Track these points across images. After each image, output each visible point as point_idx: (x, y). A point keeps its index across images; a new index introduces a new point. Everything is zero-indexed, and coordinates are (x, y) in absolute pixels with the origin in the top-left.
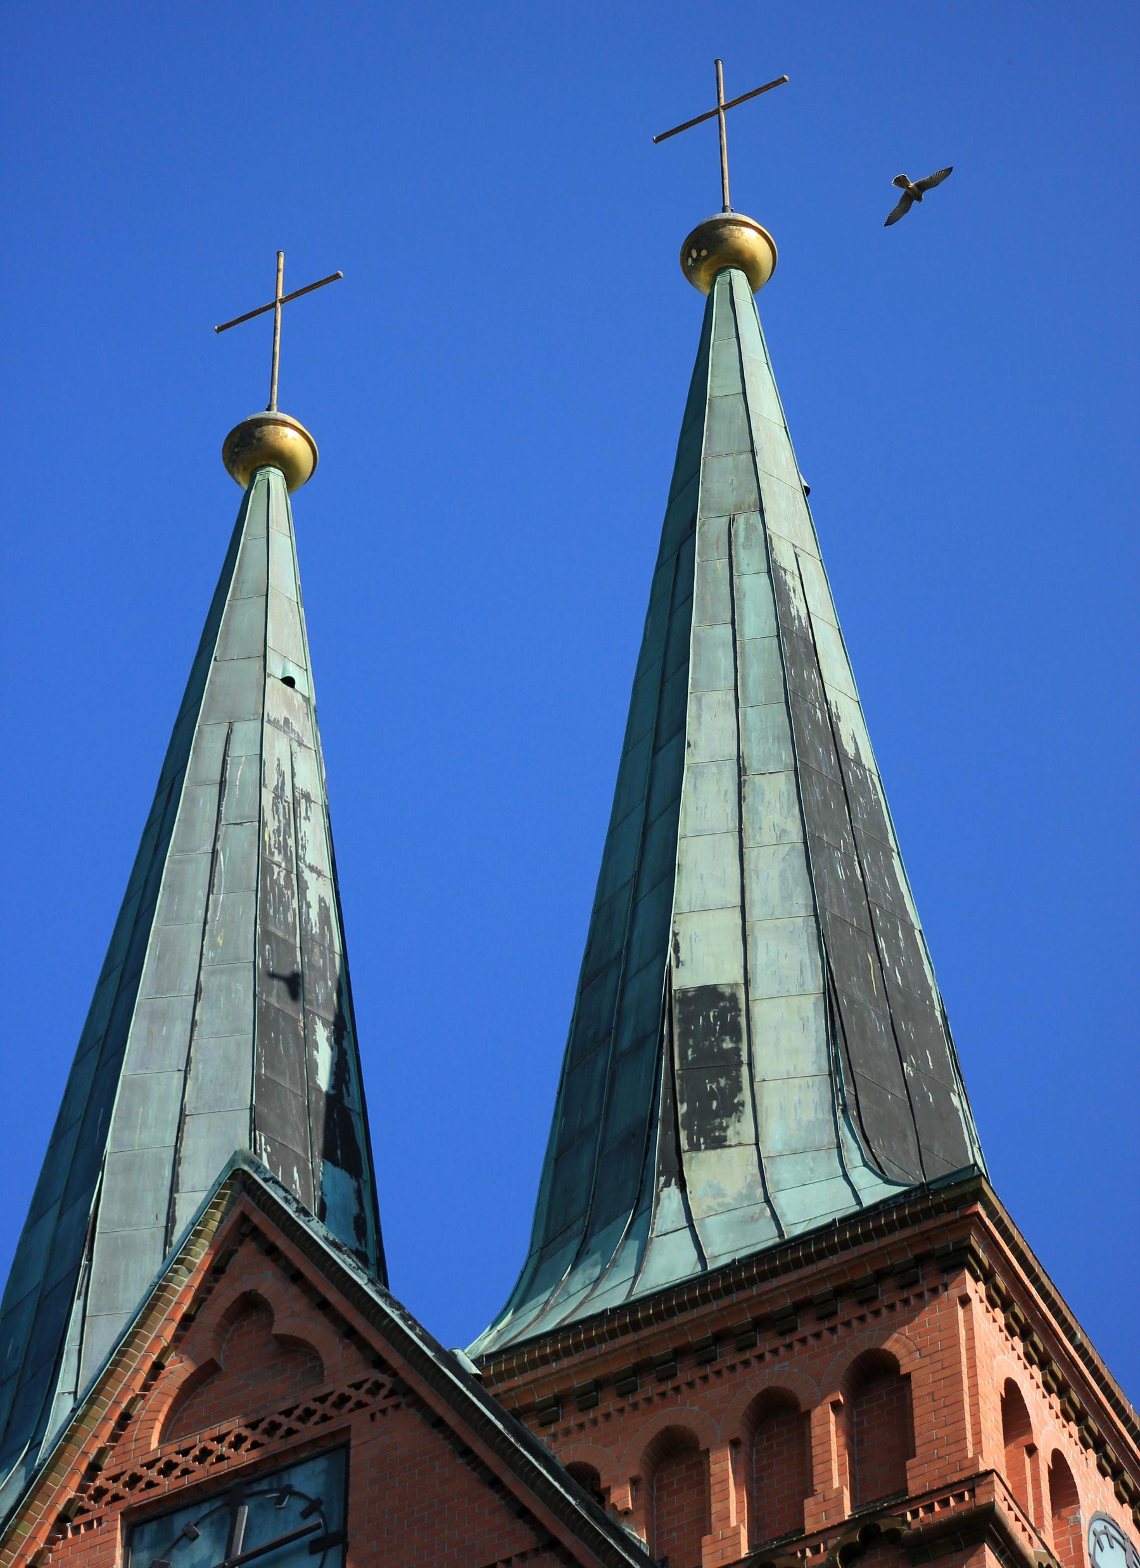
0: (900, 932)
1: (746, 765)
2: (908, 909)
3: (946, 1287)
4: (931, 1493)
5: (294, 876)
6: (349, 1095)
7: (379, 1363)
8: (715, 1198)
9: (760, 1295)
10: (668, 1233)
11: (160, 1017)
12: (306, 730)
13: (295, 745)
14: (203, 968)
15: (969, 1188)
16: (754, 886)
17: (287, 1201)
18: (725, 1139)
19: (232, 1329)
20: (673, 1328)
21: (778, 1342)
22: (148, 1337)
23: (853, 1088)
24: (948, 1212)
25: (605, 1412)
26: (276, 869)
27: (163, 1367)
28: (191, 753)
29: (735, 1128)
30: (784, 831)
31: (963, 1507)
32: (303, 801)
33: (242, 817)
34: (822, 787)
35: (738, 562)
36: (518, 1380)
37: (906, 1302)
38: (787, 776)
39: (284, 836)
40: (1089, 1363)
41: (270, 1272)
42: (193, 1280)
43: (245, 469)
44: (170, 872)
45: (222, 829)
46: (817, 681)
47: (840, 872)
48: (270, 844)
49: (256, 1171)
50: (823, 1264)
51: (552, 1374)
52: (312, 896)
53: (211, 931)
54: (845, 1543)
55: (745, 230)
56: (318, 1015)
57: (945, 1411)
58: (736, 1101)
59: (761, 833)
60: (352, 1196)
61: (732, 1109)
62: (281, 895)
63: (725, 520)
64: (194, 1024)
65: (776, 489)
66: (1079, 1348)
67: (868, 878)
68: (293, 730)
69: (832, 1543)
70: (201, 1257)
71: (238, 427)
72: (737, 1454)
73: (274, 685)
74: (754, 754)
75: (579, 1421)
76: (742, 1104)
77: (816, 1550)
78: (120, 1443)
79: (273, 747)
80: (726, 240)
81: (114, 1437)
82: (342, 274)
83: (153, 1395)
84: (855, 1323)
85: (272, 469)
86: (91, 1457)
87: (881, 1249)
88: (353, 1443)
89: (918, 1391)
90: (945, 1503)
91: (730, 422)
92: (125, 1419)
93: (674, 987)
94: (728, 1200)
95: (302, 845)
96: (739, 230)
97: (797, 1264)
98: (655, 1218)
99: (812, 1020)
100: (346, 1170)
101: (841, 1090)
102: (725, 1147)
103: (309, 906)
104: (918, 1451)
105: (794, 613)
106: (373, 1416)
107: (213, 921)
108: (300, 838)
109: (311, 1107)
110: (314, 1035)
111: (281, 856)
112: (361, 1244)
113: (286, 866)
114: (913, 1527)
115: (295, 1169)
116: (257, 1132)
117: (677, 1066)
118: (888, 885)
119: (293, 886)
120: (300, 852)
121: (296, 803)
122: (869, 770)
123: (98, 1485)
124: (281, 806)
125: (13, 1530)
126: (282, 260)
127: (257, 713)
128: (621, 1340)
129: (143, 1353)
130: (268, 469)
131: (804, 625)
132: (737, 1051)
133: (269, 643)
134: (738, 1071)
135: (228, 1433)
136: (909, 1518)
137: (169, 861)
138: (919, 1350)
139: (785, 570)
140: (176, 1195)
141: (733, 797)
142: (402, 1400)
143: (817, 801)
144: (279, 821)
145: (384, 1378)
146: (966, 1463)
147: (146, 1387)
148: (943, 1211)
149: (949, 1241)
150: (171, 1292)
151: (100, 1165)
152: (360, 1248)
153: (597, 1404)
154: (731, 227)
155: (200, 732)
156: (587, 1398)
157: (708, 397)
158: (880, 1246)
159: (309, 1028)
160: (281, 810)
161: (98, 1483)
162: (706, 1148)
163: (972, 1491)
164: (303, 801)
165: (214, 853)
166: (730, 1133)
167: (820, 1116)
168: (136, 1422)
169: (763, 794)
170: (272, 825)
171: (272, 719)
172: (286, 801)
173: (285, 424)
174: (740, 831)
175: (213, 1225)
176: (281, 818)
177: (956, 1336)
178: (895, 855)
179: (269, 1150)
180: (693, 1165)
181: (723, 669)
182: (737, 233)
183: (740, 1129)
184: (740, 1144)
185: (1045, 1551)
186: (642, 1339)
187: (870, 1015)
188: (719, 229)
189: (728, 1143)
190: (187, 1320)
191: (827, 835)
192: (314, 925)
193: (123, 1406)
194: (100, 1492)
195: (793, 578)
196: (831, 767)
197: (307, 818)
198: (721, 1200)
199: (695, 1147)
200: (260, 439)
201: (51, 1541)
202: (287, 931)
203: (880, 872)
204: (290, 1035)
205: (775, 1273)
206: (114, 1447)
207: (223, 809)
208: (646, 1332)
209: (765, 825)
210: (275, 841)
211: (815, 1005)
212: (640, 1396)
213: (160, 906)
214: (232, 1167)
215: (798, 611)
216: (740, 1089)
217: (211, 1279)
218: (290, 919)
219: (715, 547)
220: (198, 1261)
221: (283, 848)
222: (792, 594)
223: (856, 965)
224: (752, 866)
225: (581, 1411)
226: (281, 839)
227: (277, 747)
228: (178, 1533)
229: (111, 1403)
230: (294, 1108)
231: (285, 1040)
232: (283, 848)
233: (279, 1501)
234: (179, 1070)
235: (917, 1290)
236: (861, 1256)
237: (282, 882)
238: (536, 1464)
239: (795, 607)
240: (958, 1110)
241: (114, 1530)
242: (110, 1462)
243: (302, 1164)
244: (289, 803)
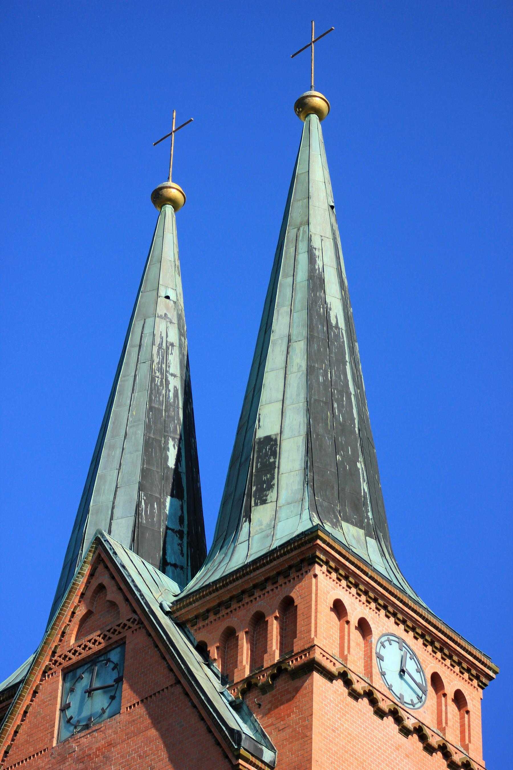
0: (344, 398)
1: (291, 338)
2: (350, 386)
3: (310, 570)
4: (303, 651)
5: (164, 380)
6: (181, 467)
7: (134, 612)
8: (259, 526)
9: (254, 577)
10: (242, 543)
11: (112, 447)
12: (174, 316)
13: (169, 323)
14: (128, 425)
15: (314, 535)
16: (288, 391)
17: (110, 549)
18: (266, 500)
19: (97, 596)
20: (228, 590)
21: (260, 593)
22: (70, 603)
23: (312, 473)
24: (309, 543)
25: (210, 621)
26: (157, 379)
27: (75, 613)
28: (130, 334)
29: (270, 495)
30: (301, 366)
31: (306, 659)
32: (170, 347)
33: (145, 360)
34: (318, 343)
35: (298, 248)
36: (183, 611)
37: (298, 576)
38: (304, 342)
39: (161, 364)
40: (376, 581)
41: (107, 576)
42: (84, 580)
43: (159, 206)
44: (120, 386)
45: (139, 365)
46: (323, 295)
47: (321, 379)
48: (155, 369)
49: (102, 537)
50: (272, 564)
51: (193, 608)
52: (171, 387)
53: (132, 409)
54: (272, 673)
55: (314, 98)
56: (170, 436)
57: (306, 620)
58: (272, 484)
59: (293, 367)
60: (179, 508)
61: (270, 487)
62: (158, 389)
63: (296, 230)
64: (123, 449)
65: (317, 212)
66: (371, 578)
67: (334, 378)
68: (168, 318)
69: (268, 673)
70: (86, 571)
71: (154, 191)
72: (248, 636)
73: (162, 300)
74: (295, 332)
75: (203, 624)
76: (274, 485)
77: (263, 676)
78: (62, 642)
79: (159, 327)
80: (307, 104)
81: (60, 640)
82: (192, 119)
83: (72, 624)
84: (283, 585)
85: (167, 205)
86: (53, 649)
87: (289, 558)
88: (127, 642)
89: (299, 612)
90: (301, 657)
91: (303, 185)
92: (63, 633)
93: (257, 437)
94: (263, 527)
95: (169, 366)
96: (312, 99)
97: (264, 565)
98: (239, 536)
99: (301, 447)
100: (177, 498)
101: (307, 475)
102: (266, 503)
103: (169, 391)
104: (298, 635)
105: (317, 267)
106: (133, 632)
107: (133, 405)
108: (168, 363)
109: (164, 476)
110: (168, 445)
111: (159, 373)
112: (181, 527)
113: (161, 377)
114: (291, 667)
115: (155, 503)
116: (141, 492)
117: (254, 471)
118: (342, 378)
119: (163, 384)
120: (168, 369)
121: (167, 348)
122: (341, 329)
123: (55, 659)
124: (161, 352)
125: (28, 679)
126: (175, 114)
127: (154, 314)
128: (213, 595)
129: (68, 609)
130: (166, 206)
131: (321, 271)
132: (275, 462)
133: (160, 283)
134: (274, 471)
135: (92, 639)
136: (291, 663)
137: (120, 381)
138: (300, 596)
139: (315, 249)
140: (112, 521)
141: (285, 353)
142: (141, 626)
143: (315, 350)
144: (159, 358)
145: (136, 617)
146: (311, 640)
147: (70, 621)
148: (307, 543)
149: (309, 554)
150: (77, 585)
151: (88, 512)
152: (181, 529)
153: (208, 618)
154: (309, 98)
155: (134, 324)
156: (204, 616)
157: (296, 174)
158: (284, 560)
159: (166, 443)
160: (161, 354)
161: (55, 658)
162: (260, 505)
163: (309, 653)
164: (170, 347)
165: (135, 376)
166: (269, 497)
167: (299, 487)
168: (67, 634)
169: (295, 350)
170: (156, 360)
171: (159, 315)
172: (163, 349)
173: (170, 187)
174: (286, 367)
175: (90, 558)
176: (160, 357)
177: (311, 591)
178: (348, 364)
179: (145, 498)
180: (255, 512)
181: (288, 297)
182: (311, 101)
183: (272, 496)
184: (271, 502)
185: (343, 666)
186: (220, 594)
187: (325, 438)
188: (304, 100)
189: (267, 502)
190: (82, 595)
191: (317, 364)
192: (171, 399)
193: (63, 629)
194: (56, 661)
195: (319, 251)
196: (324, 333)
197: (172, 354)
198: (260, 527)
199: (256, 504)
200: (161, 195)
201: (41, 680)
202: (160, 404)
203: (339, 373)
204: (158, 448)
205: (257, 568)
206: (60, 644)
207: (139, 357)
208: (220, 592)
209: (295, 364)
210: (157, 368)
211: (303, 440)
212: (220, 615)
213: (116, 400)
214: (95, 536)
215: (319, 266)
216: (274, 478)
217: (90, 578)
218: (161, 399)
219: (291, 243)
220: (85, 572)
221: (160, 370)
222: (317, 259)
223: (322, 419)
224: (288, 382)
225: (203, 621)
226: (160, 366)
227: (161, 326)
228: (78, 677)
229: (58, 628)
230: (157, 478)
231: (156, 451)
232: (160, 370)
233: (106, 664)
234: (117, 469)
235: (301, 572)
236: (283, 561)
237: (159, 384)
238: (174, 652)
239: (318, 264)
240: (359, 469)
241: (58, 676)
242: (59, 650)
243: (158, 501)
244: (164, 349)
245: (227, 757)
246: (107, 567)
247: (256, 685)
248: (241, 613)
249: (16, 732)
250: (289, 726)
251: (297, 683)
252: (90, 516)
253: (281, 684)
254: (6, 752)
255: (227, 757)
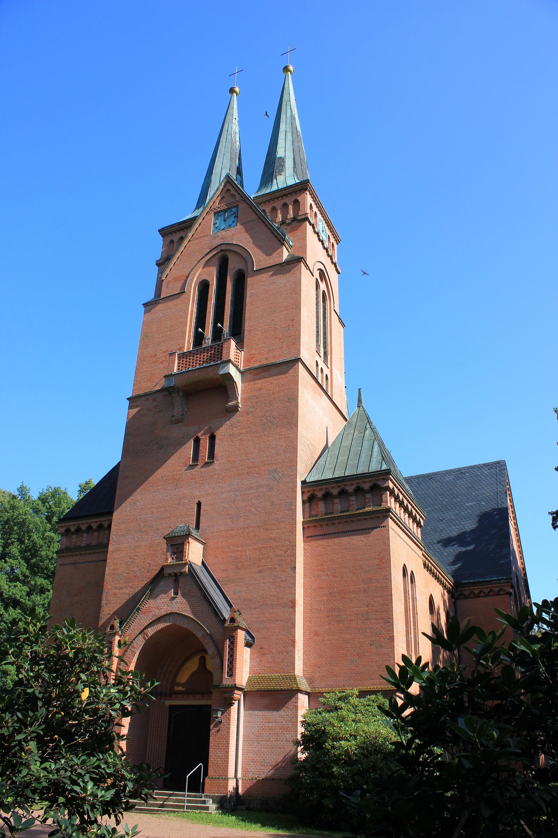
7: (242, 197)
61: (282, 171)
73: (234, 119)
92: (214, 202)
151: (212, 173)
156: (265, 202)
170: (233, 136)
183: (283, 173)
227: (234, 126)
245: (280, 241)
246: (231, 184)
247: (286, 223)
248: (279, 202)
249: (196, 229)
250: (297, 236)
251: (300, 224)
252: (213, 175)
253: (295, 223)
254: (193, 235)
255: (280, 241)
